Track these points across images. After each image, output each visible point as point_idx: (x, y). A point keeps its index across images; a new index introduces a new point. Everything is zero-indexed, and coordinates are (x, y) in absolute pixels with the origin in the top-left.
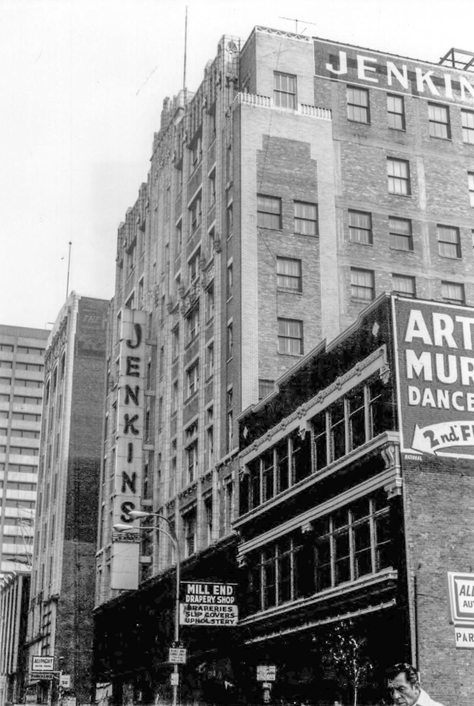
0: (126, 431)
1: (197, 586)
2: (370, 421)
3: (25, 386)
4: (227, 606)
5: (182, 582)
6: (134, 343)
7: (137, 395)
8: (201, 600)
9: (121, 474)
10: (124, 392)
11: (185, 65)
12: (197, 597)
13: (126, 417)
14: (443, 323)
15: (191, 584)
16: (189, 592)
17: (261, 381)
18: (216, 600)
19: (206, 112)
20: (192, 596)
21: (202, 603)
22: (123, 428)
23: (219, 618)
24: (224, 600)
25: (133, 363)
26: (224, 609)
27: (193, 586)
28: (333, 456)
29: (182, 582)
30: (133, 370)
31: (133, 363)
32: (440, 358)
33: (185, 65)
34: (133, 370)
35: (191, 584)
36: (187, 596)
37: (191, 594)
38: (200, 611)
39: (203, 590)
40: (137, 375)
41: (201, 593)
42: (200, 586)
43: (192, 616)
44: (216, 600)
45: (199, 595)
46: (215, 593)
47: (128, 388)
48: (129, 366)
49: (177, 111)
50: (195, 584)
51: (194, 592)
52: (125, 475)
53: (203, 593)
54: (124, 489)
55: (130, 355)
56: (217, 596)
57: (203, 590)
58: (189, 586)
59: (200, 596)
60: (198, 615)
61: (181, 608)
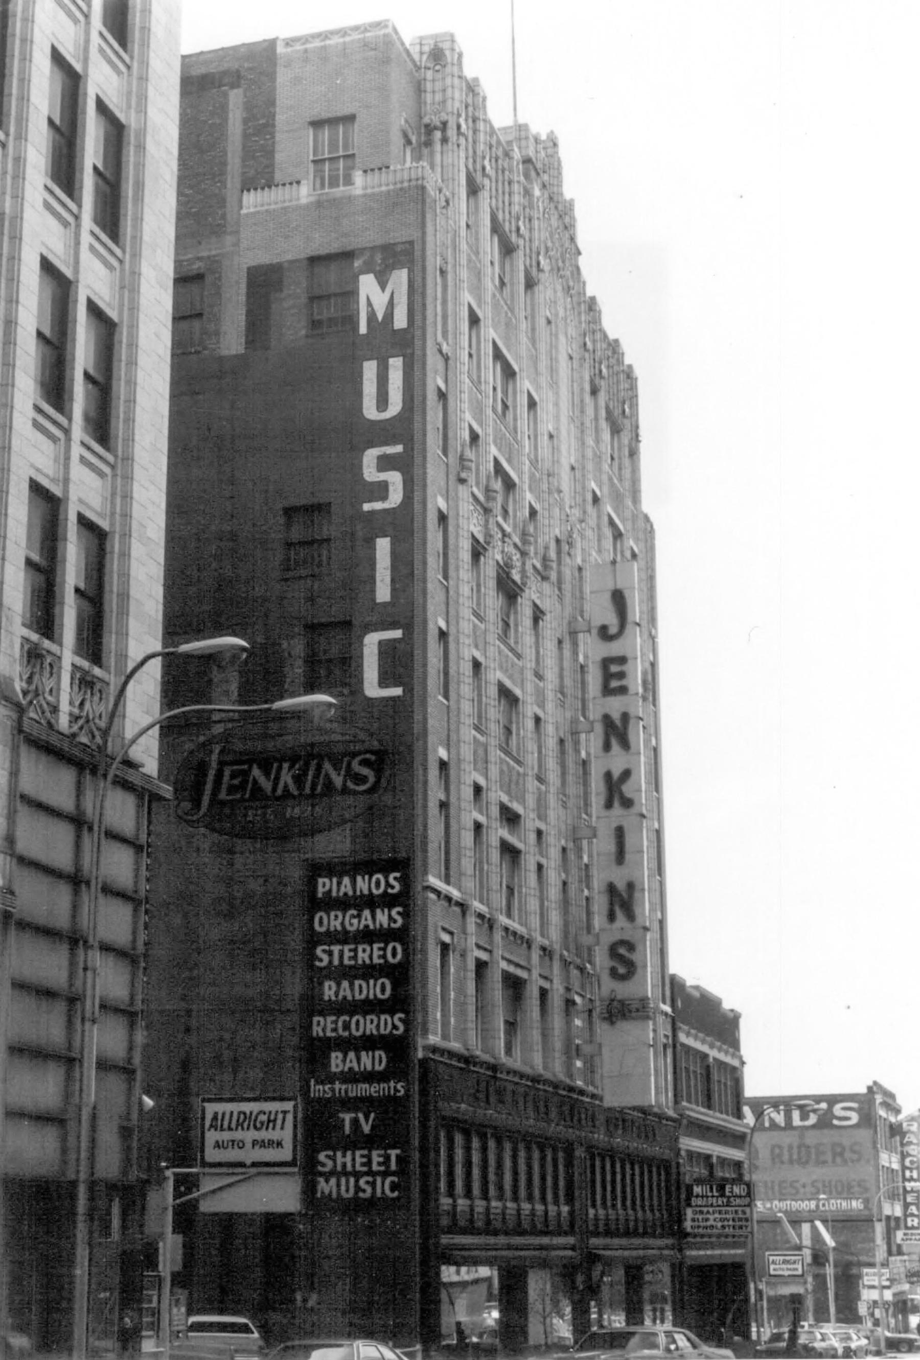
0: (609, 805)
4: (740, 1209)
6: (613, 630)
7: (611, 904)
9: (603, 887)
10: (599, 728)
11: (514, 88)
13: (608, 775)
18: (728, 1201)
19: (902, 1293)
21: (712, 1205)
22: (602, 800)
23: (731, 1223)
24: (738, 1201)
25: (614, 669)
26: (736, 1212)
30: (614, 684)
31: (614, 669)
33: (514, 88)
34: (614, 684)
37: (697, 1196)
40: (623, 690)
44: (728, 1201)
46: (727, 1194)
47: (607, 720)
48: (608, 676)
52: (611, 889)
54: (611, 917)
55: (605, 654)
56: (729, 1197)
61: (689, 1212)
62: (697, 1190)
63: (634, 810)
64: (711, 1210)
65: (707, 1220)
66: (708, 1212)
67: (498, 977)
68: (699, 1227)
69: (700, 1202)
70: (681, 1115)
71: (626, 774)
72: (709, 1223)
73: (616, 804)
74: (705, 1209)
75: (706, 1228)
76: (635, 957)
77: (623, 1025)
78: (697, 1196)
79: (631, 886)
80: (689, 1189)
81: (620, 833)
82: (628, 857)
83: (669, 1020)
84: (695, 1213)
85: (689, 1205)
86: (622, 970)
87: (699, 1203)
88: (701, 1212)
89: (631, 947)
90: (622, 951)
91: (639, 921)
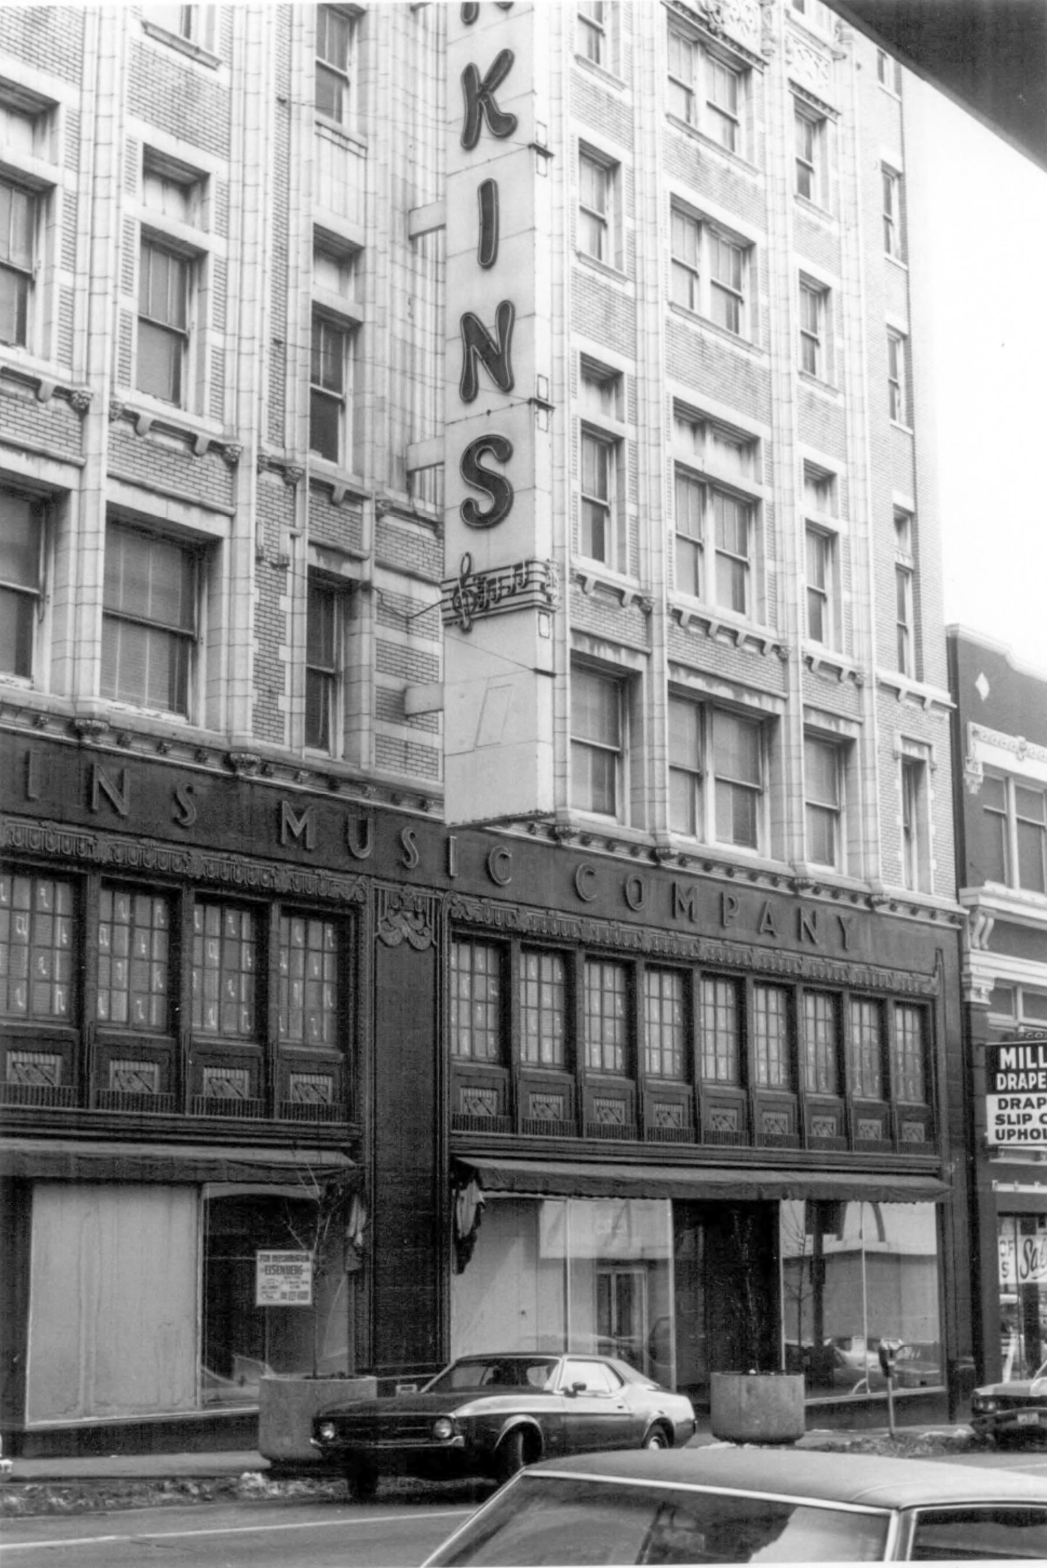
1: (1021, 1050)
2: (935, 1062)
3: (533, 315)
5: (784, 1367)
8: (1032, 1084)
12: (1022, 1076)
14: (577, 1390)
15: (1008, 1048)
16: (1003, 1066)
17: (291, 6)
20: (1011, 1075)
21: (1035, 1089)
27: (1013, 1051)
28: (1030, 991)
29: (784, 1367)
32: (1021, 1066)
35: (1008, 1048)
36: (999, 1076)
37: (1008, 1070)
38: (1029, 1110)
39: (1035, 1059)
41: (1031, 1065)
42: (1029, 1050)
43: (1010, 1123)
45: (1027, 1071)
49: (423, 805)
50: (1017, 1047)
51: (1014, 1066)
53: (1034, 1066)
57: (1035, 1059)
58: (1003, 1051)
59: (1031, 1075)
60: (1025, 1121)
61: (992, 1102)
62: (1007, 1058)
63: (523, 135)
64: (1033, 1097)
65: (1027, 1118)
66: (1029, 1103)
67: (96, 519)
68: (1011, 1134)
69: (1011, 1081)
70: (973, 908)
71: (504, 62)
72: (1029, 1126)
73: (485, 131)
74: (1023, 1097)
75: (1023, 1134)
76: (512, 472)
77: (485, 632)
78: (1008, 1070)
79: (505, 311)
80: (993, 1055)
81: (488, 192)
82: (506, 249)
83: (947, 716)
84: (1002, 1105)
85: (993, 1090)
86: (485, 505)
87: (1012, 1084)
88: (1016, 1103)
89: (502, 448)
90: (488, 462)
91: (523, 389)
